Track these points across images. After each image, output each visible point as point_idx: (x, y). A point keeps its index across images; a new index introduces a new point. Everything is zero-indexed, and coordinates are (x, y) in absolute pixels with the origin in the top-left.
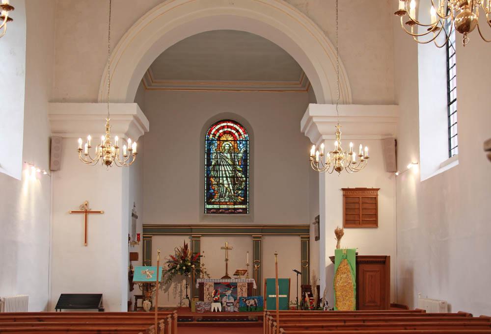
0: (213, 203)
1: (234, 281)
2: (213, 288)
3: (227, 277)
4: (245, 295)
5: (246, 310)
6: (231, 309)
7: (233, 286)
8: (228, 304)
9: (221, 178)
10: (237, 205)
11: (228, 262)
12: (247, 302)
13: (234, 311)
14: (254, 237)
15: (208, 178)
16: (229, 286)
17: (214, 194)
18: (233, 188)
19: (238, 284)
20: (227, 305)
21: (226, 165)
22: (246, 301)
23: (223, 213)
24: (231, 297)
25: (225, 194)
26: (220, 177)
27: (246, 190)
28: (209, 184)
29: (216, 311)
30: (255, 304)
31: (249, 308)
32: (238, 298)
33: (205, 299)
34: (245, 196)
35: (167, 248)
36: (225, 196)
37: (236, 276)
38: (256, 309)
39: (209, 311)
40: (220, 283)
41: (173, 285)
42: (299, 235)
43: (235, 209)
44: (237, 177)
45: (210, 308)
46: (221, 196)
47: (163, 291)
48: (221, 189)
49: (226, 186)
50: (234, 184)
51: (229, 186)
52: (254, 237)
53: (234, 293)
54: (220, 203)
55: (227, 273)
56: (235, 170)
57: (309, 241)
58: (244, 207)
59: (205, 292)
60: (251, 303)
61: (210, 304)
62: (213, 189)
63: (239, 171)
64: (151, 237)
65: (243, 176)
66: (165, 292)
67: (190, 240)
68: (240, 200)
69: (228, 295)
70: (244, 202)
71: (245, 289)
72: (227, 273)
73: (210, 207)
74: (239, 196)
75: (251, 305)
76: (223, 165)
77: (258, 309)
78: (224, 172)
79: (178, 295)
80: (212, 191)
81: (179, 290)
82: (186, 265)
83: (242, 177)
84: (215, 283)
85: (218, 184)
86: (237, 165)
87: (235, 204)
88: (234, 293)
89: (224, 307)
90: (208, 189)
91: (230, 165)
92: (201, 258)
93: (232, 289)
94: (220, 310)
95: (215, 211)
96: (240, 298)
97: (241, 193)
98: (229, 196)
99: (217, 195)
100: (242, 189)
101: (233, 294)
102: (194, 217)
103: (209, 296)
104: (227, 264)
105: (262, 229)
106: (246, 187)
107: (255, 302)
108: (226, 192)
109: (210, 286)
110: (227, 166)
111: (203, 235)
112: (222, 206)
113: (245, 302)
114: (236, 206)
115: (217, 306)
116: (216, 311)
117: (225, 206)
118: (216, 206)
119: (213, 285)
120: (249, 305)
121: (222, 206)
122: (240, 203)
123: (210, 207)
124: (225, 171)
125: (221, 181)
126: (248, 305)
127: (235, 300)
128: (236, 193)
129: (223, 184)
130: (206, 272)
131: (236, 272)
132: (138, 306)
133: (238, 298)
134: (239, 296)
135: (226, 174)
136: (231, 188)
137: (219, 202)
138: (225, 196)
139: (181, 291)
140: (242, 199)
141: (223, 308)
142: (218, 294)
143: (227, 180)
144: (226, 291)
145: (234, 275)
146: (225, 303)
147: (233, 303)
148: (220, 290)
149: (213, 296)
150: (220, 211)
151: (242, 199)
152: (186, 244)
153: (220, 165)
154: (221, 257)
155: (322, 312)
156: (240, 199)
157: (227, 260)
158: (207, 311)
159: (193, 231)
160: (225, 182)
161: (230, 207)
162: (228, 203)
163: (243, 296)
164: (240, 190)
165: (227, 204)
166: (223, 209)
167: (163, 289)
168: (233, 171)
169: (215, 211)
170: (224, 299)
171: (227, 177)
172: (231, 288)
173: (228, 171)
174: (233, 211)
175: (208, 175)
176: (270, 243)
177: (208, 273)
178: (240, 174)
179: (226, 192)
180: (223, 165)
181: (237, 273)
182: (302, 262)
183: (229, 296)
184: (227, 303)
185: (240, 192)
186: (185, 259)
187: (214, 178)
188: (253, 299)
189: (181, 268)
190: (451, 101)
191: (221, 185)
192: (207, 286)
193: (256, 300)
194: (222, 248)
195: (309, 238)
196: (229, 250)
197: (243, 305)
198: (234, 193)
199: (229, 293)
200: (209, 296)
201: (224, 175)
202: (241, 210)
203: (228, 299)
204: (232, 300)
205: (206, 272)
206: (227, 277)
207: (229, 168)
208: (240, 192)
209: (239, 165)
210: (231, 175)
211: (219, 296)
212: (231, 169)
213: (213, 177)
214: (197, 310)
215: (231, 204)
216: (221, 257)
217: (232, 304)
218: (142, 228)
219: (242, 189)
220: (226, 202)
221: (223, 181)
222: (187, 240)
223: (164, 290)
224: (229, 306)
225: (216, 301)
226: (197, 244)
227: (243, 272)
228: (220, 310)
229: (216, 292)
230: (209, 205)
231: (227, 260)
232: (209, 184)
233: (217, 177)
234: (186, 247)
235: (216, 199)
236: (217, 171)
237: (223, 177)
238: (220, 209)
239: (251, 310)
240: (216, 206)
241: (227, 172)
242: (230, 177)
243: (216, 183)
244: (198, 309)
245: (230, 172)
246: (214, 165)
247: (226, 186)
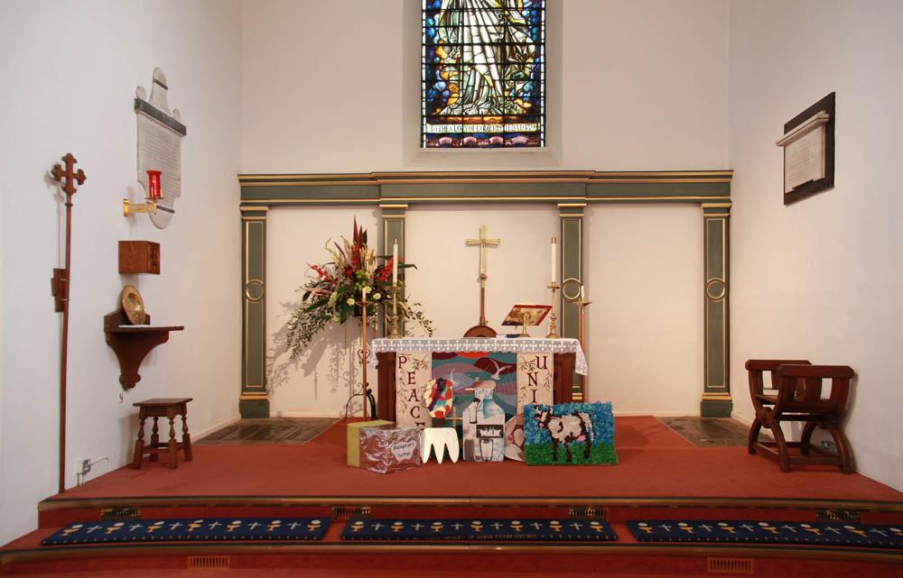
0: (445, 120)
1: (505, 348)
2: (428, 372)
3: (482, 330)
4: (546, 398)
5: (549, 459)
6: (492, 450)
7: (501, 365)
8: (483, 433)
9: (466, 48)
10: (511, 122)
11: (487, 285)
12: (554, 424)
13: (506, 458)
14: (563, 210)
15: (431, 46)
16: (486, 364)
17: (447, 93)
18: (500, 74)
19: (520, 361)
20: (478, 435)
21: (480, 10)
22: (549, 419)
23: (474, 146)
24: (494, 406)
25: (478, 94)
26: (463, 45)
27: (537, 81)
28: (433, 65)
29: (440, 458)
30: (584, 432)
31: (561, 451)
32: (520, 411)
33: (399, 415)
34: (535, 97)
35: (306, 245)
36: (478, 97)
37: (511, 330)
38: (587, 454)
39: (413, 463)
40: (453, 355)
41: (329, 352)
42: (699, 203)
43: (505, 135)
44: (512, 44)
45: (417, 452)
46: (465, 100)
47: (302, 371)
48: (466, 79)
49: (482, 69)
50: (504, 64)
51: (489, 70)
52: (563, 210)
53: (506, 391)
54: (463, 119)
55: (482, 317)
56: (506, 24)
57: (728, 218)
58: (531, 128)
59: (399, 386)
60: (567, 432)
61: (415, 436)
62: (444, 80)
63: (517, 26)
64: (264, 213)
65: (529, 40)
66: (306, 375)
67: (376, 220)
68: (520, 110)
69: (481, 397)
70: (532, 115)
71: (545, 376)
72: (482, 317)
73: (437, 129)
74: (517, 97)
75: (570, 438)
76: (473, 10)
77: (595, 456)
78: (474, 31)
79: (342, 382)
80: (443, 84)
81: (346, 367)
82: (361, 295)
83: (524, 44)
84: (436, 356)
85: (459, 65)
86: (511, 8)
87: (506, 119)
88: (506, 391)
89: (470, 443)
90: (431, 80)
91: (491, 9)
92: (406, 269)
93: (496, 376)
94: (454, 457)
95: (449, 140)
96: (527, 410)
97: (522, 89)
98: (489, 99)
99: (454, 95)
100: (527, 78)
101: (500, 395)
102: (385, 142)
103: (413, 403)
104: (483, 290)
105: (586, 184)
106: (537, 72)
107: (582, 424)
108: (481, 87)
109: (417, 364)
110: (484, 13)
111: (412, 205)
112: (468, 128)
113: (546, 423)
114: (509, 128)
115: (439, 441)
116: (440, 458)
117: (479, 128)
118: (451, 128)
119: (429, 359)
120: (561, 437)
121: (468, 128)
122: (522, 119)
123: (437, 129)
124: (478, 26)
125: (467, 58)
126: (556, 436)
127: (508, 417)
128: (510, 90)
129: (472, 65)
130: (419, 315)
131: (512, 314)
132: (161, 441)
133: (520, 411)
134: (523, 400)
135: (479, 35)
136: (496, 77)
137: (461, 115)
138: (478, 97)
139: (352, 372)
140: (527, 105)
141: (465, 447)
142: (448, 396)
143: (484, 51)
144: (476, 385)
145: (505, 323)
146: (473, 429)
147: (499, 427)
148: (455, 382)
149: (429, 402)
150: (465, 140)
151: (527, 105)
152: (363, 232)
153: (463, 10)
154: (466, 269)
155: (250, 220)
156: (521, 106)
157: (483, 278)
158: (405, 464)
159: (385, 193)
160: (480, 59)
161: (494, 128)
162: (486, 119)
163: (539, 402)
164: (518, 79)
165: (483, 122)
166: (471, 134)
167: (300, 364)
168: (500, 25)
169: (449, 140)
170: (470, 415)
171: (483, 44)
172: (494, 371)
173: (486, 26)
174: (501, 140)
175: (430, 39)
176: (609, 227)
177: (425, 316)
178: (519, 36)
179: (481, 87)
180: (473, 10)
181: (515, 318)
182: (706, 284)
183: (486, 401)
184: (480, 427)
185: (519, 86)
186: (354, 275)
187: (447, 49)
188: (576, 414)
189: (341, 303)
190: (544, 310)
191: (466, 68)
192: (408, 367)
193: (585, 417)
194: (469, 244)
195: (728, 209)
196: (489, 250)
197: (537, 438)
198: (504, 89)
199: (485, 390)
200: (413, 403)
201: (476, 40)
202: (522, 139)
203: (483, 412)
204: (498, 417)
205: (419, 315)
206: (482, 330)
207: (491, 19)
208: (519, 86)
209: (516, 9)
210: (494, 38)
211: (450, 402)
212: (496, 22)
213: (443, 45)
214: (365, 463)
215: (495, 122)
216: (466, 269)
217: (497, 433)
218: (238, 186)
219: (527, 78)
220: (482, 116)
221: (473, 56)
222: (368, 220)
223: (304, 366)
224: (487, 439)
225: (439, 422)
226: (395, 231)
227: (534, 312)
228: (454, 457)
229: (441, 385)
230: (432, 124)
231: (483, 278)
232: (433, 65)
233: (457, 45)
234: (361, 238)
235: (453, 107)
236: (455, 27)
237: (471, 44)
238: (463, 135)
239: (569, 460)
240: (451, 128)
241: (483, 29)
242: (491, 44)
243: (453, 62)
244: (371, 458)
245: (492, 29)
246: (449, 11)
247: (482, 69)
